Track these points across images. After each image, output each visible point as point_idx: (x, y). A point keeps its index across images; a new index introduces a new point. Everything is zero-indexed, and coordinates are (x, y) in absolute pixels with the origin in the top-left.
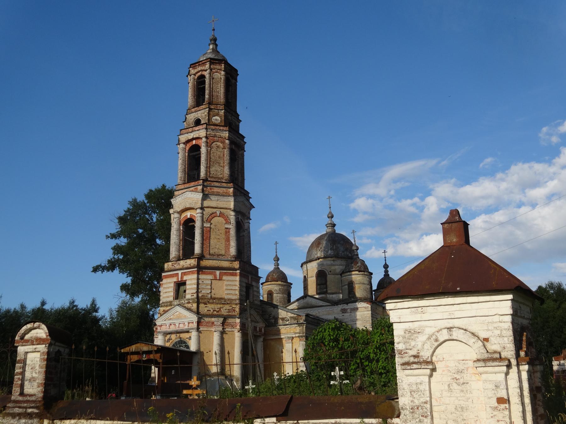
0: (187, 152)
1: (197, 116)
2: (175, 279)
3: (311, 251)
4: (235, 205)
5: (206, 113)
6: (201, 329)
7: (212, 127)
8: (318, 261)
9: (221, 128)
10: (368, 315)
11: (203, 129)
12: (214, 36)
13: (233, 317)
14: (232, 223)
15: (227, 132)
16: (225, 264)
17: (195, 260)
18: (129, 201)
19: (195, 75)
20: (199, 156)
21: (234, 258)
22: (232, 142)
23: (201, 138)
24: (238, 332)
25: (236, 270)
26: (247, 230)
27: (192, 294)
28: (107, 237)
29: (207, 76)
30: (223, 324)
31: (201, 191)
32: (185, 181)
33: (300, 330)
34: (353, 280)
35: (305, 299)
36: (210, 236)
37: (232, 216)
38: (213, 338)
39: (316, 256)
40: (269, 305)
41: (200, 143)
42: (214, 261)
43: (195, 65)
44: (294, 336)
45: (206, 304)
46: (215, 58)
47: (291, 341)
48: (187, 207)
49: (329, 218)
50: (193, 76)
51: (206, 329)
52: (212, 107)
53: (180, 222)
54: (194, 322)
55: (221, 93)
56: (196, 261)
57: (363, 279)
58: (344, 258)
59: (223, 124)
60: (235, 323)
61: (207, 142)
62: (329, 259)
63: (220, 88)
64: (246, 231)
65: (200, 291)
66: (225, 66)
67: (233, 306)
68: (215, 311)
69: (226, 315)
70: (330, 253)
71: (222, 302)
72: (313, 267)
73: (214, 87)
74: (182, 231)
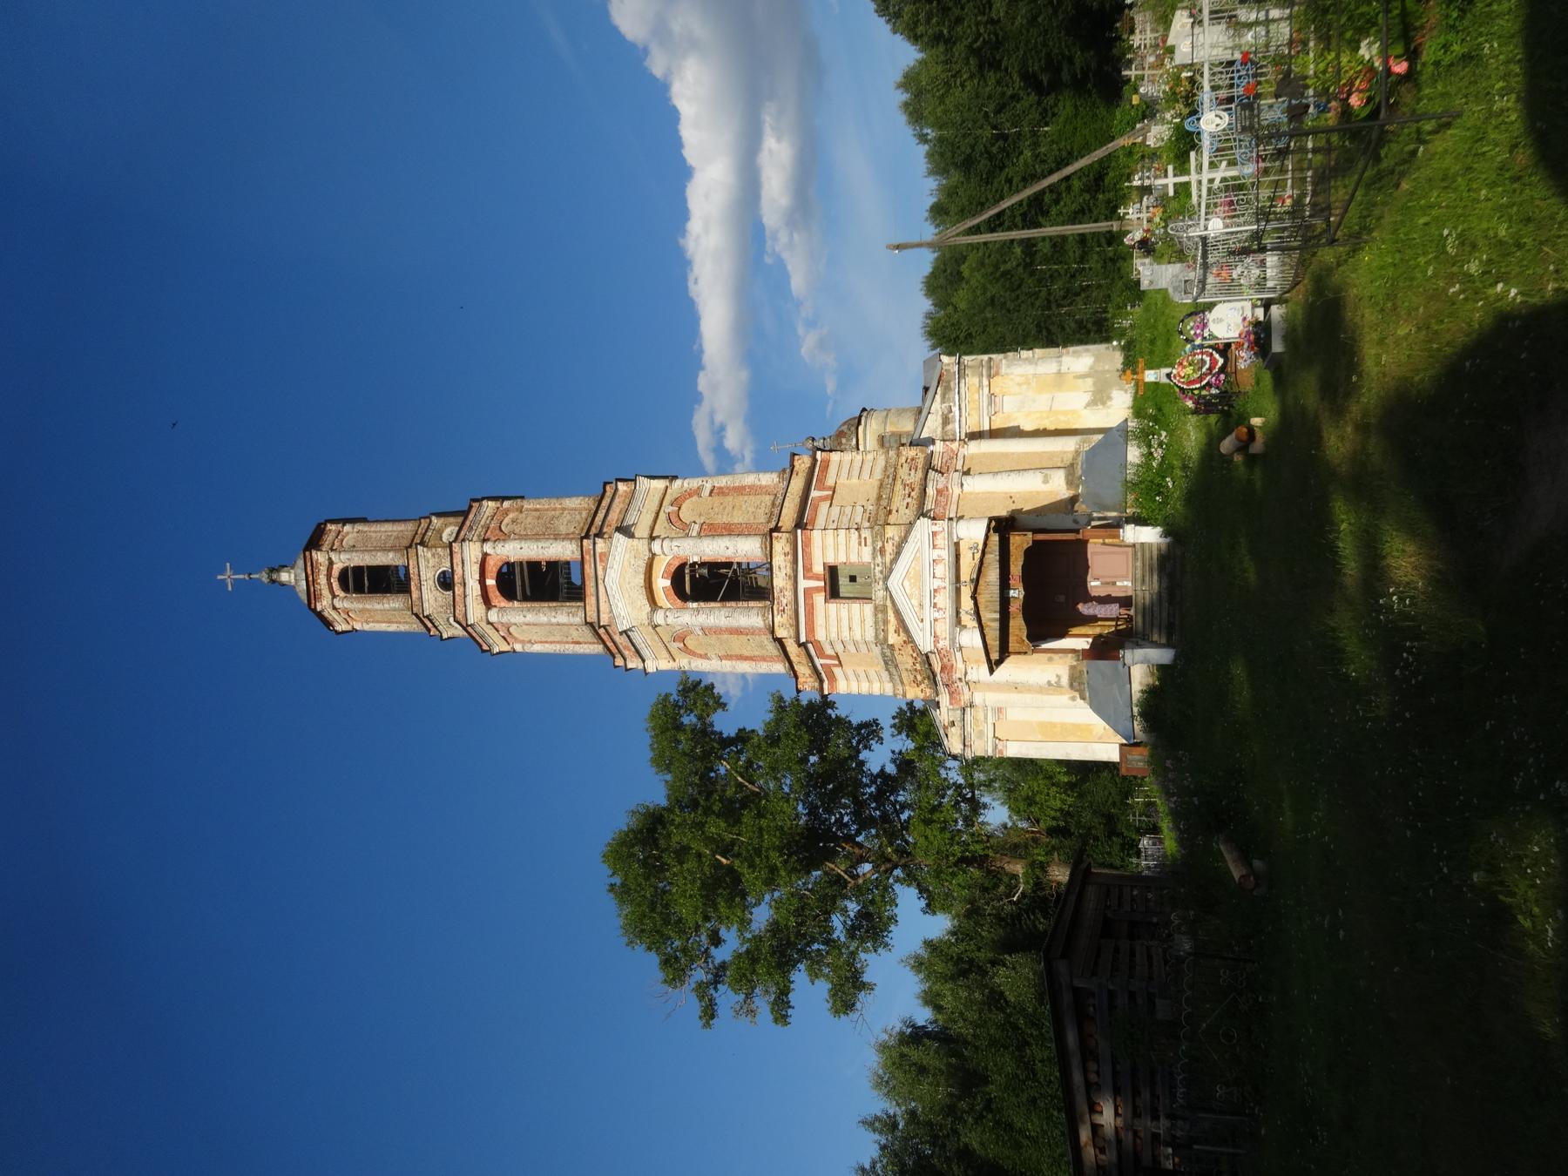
1: (431, 582)
2: (819, 599)
11: (464, 547)
14: (700, 483)
17: (777, 538)
18: (627, 945)
19: (334, 596)
27: (860, 544)
33: (973, 376)
45: (890, 512)
48: (642, 581)
50: (336, 602)
54: (935, 528)
63: (379, 534)
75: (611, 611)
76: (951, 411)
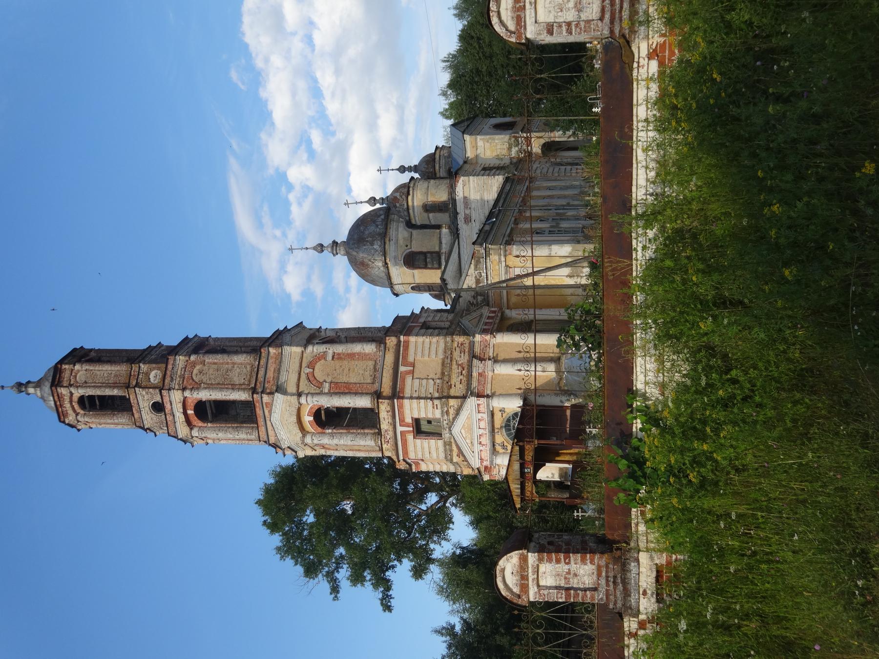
0: (206, 425)
1: (147, 409)
2: (410, 437)
3: (374, 278)
4: (297, 346)
5: (144, 393)
6: (489, 392)
7: (166, 381)
8: (389, 266)
9: (170, 367)
10: (476, 181)
11: (171, 394)
12: (12, 387)
13: (472, 345)
14: (325, 350)
15: (177, 357)
16: (390, 358)
18: (281, 560)
19: (77, 414)
20: (212, 402)
21: (380, 346)
22: (196, 351)
23: (185, 398)
24: (495, 337)
25: (399, 341)
26: (337, 332)
27: (433, 408)
28: (336, 598)
29: (81, 392)
30: (481, 359)
31: (271, 396)
32: (253, 427)
33: (495, 255)
34: (421, 204)
35: (446, 282)
36: (344, 383)
37: (313, 350)
38: (503, 375)
39: (382, 269)
40: (456, 304)
41: (192, 402)
42: (384, 374)
43: (61, 414)
44: (503, 264)
45: (450, 387)
46: (50, 381)
47: (511, 269)
48: (295, 420)
49: (323, 251)
50: (79, 418)
51: (489, 386)
52: (134, 383)
53: (319, 433)
54: (479, 402)
55: (111, 370)
56: (384, 401)
57: (421, 189)
58: (386, 225)
59: (164, 366)
60: (482, 343)
61: (191, 389)
62: (387, 247)
64: (338, 334)
65: (430, 396)
66: (66, 364)
67: (456, 345)
68: (461, 372)
69: (469, 356)
70: (377, 246)
71: (449, 362)
72: (400, 274)
73: (101, 381)
74: (335, 431)
75: (276, 436)
76: (481, 276)
